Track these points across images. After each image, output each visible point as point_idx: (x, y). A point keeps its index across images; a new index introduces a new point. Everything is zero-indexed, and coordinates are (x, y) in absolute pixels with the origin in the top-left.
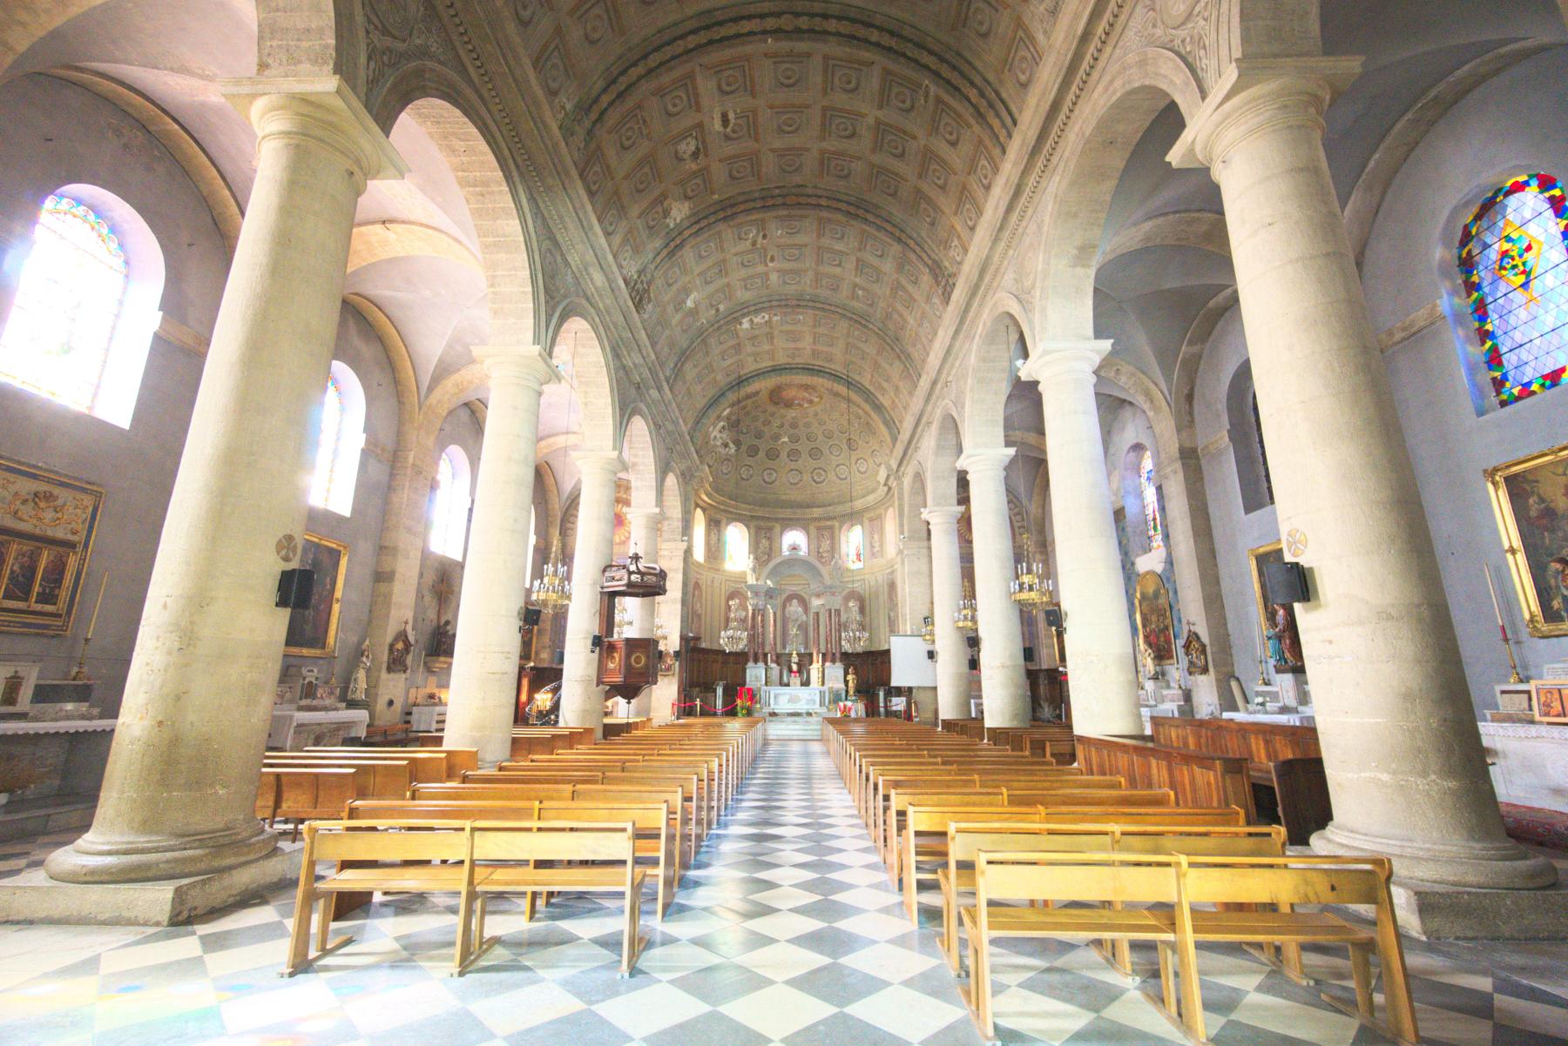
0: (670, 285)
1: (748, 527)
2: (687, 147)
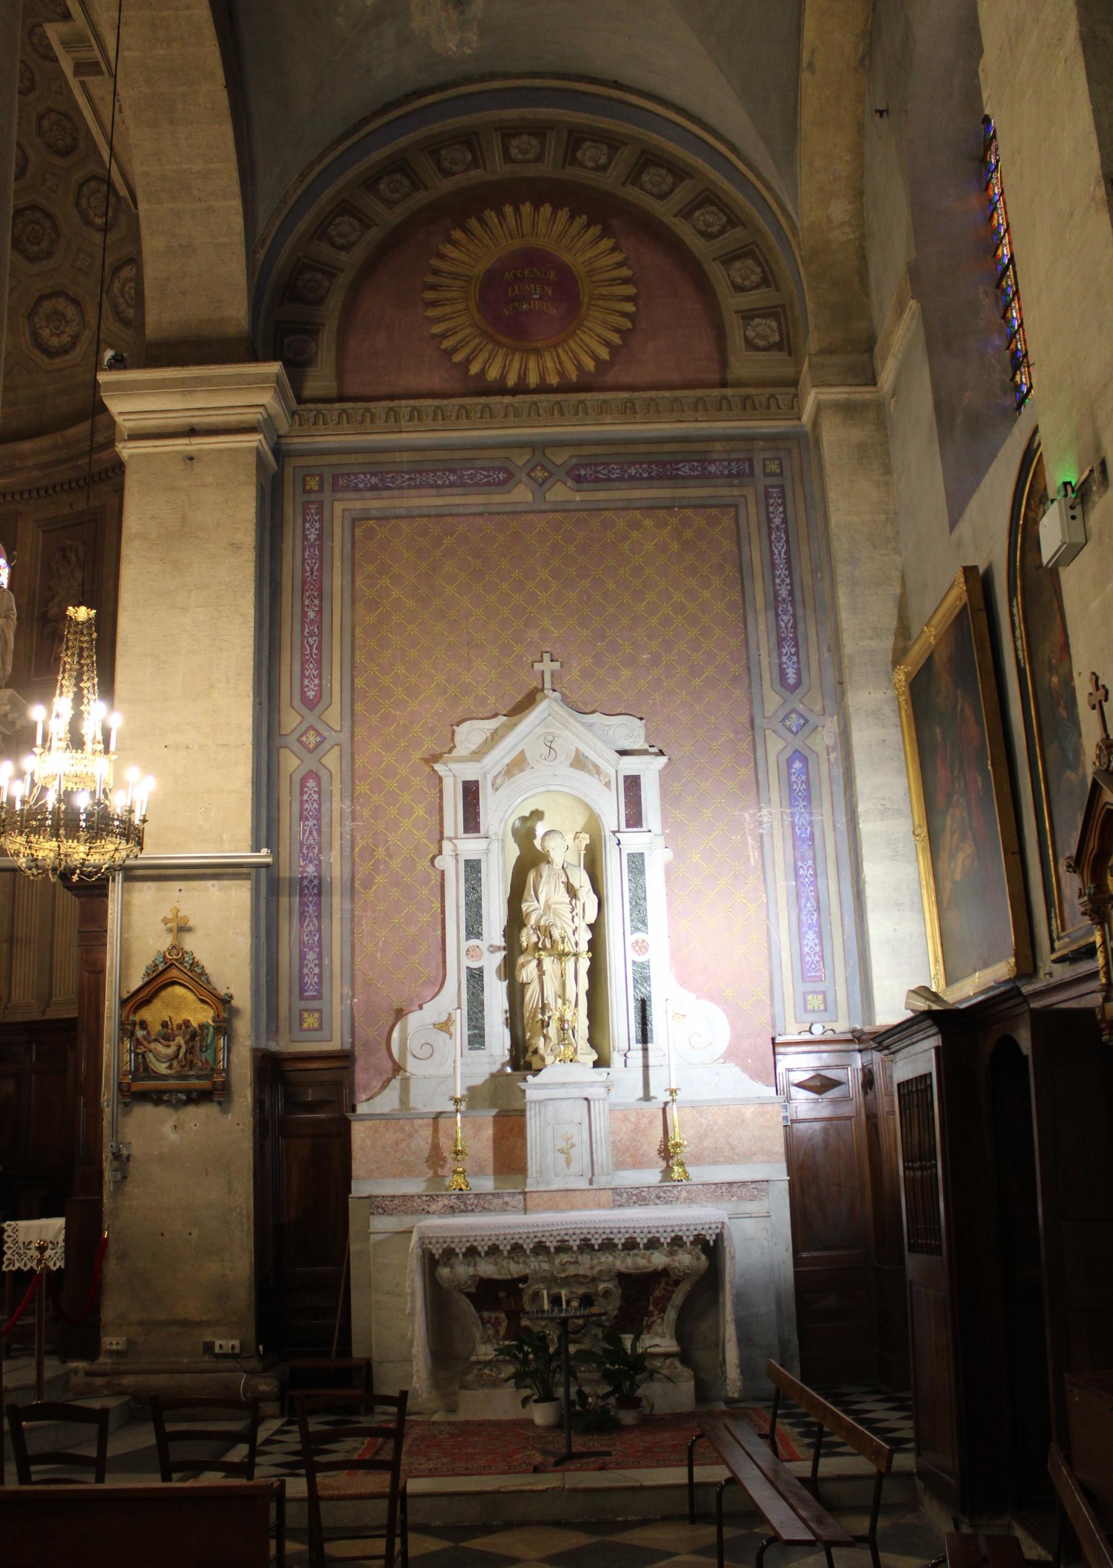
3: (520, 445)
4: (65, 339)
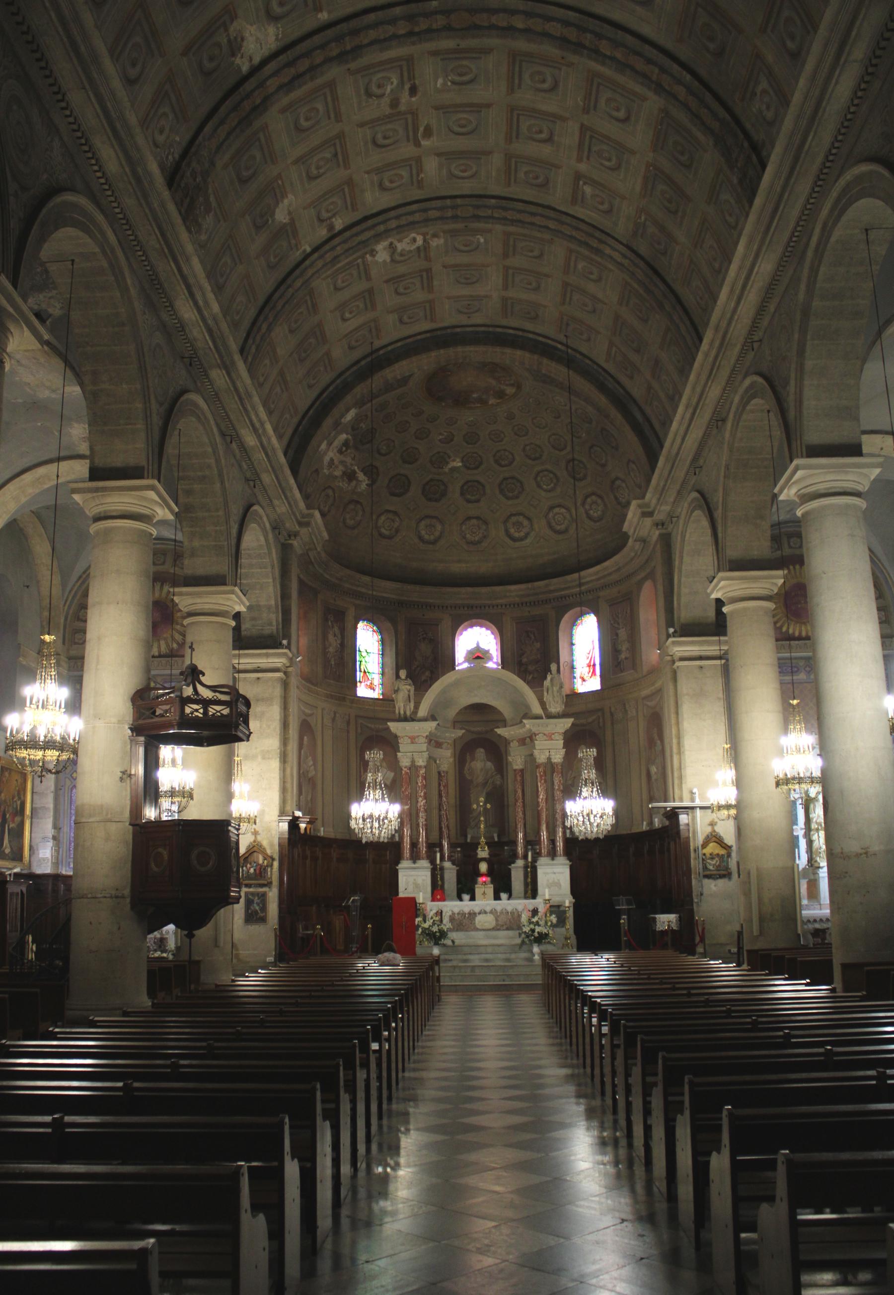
0: (244, 181)
1: (381, 631)
3: (801, 658)
4: (522, 534)
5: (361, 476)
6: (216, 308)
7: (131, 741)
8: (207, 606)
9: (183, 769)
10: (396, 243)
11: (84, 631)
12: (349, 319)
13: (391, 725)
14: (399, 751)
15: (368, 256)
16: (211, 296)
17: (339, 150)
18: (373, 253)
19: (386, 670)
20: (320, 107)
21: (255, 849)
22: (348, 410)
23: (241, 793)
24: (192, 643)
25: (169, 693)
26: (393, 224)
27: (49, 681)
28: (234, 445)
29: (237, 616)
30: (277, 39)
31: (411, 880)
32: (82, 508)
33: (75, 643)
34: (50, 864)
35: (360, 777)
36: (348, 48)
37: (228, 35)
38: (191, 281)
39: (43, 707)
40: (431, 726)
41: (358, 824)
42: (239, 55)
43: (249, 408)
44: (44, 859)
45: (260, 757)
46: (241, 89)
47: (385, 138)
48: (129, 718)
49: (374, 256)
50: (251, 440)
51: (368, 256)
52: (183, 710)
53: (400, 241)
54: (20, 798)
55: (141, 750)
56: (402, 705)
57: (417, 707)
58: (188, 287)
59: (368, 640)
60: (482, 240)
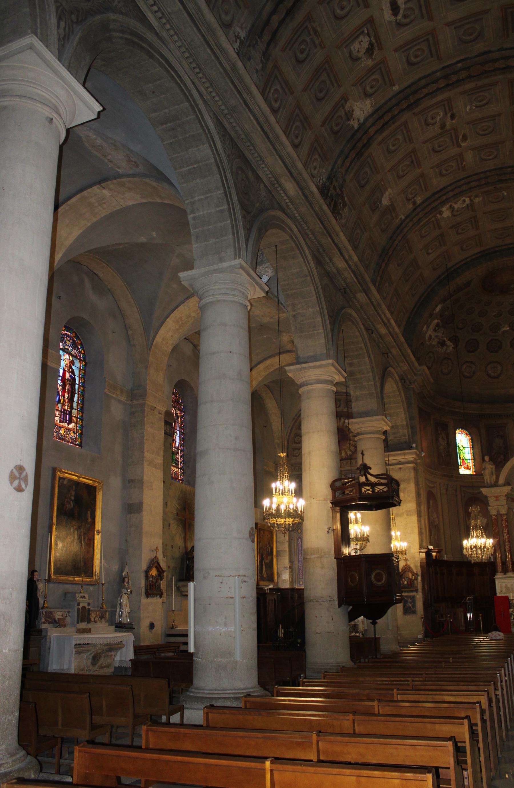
0: (362, 187)
2: (360, 46)
5: (448, 343)
6: (356, 259)
7: (332, 510)
8: (368, 429)
9: (362, 525)
10: (453, 204)
11: (300, 449)
12: (431, 253)
13: (482, 489)
14: (489, 506)
15: (438, 215)
16: (352, 252)
17: (414, 158)
18: (441, 213)
19: (476, 457)
20: (400, 137)
21: (406, 569)
22: (436, 306)
23: (396, 536)
24: (362, 451)
25: (352, 481)
26: (451, 194)
27: (284, 479)
28: (374, 335)
29: (385, 433)
30: (372, 106)
31: (504, 585)
32: (293, 380)
33: (294, 456)
34: (289, 582)
35: (466, 522)
36: (412, 101)
37: (345, 110)
38: (341, 246)
39: (282, 494)
40: (507, 489)
41: (468, 552)
42: (352, 119)
43: (381, 313)
44: (285, 580)
45: (405, 515)
46: (355, 137)
47: (440, 146)
48: (330, 497)
49: (441, 214)
50: (383, 331)
51: (438, 215)
52: (361, 490)
53: (456, 203)
54: (270, 546)
55: (338, 515)
56: (488, 478)
57: (498, 477)
58: (339, 250)
59: (462, 440)
60: (506, 194)
